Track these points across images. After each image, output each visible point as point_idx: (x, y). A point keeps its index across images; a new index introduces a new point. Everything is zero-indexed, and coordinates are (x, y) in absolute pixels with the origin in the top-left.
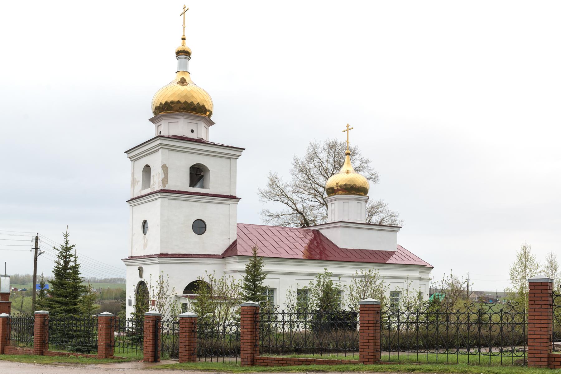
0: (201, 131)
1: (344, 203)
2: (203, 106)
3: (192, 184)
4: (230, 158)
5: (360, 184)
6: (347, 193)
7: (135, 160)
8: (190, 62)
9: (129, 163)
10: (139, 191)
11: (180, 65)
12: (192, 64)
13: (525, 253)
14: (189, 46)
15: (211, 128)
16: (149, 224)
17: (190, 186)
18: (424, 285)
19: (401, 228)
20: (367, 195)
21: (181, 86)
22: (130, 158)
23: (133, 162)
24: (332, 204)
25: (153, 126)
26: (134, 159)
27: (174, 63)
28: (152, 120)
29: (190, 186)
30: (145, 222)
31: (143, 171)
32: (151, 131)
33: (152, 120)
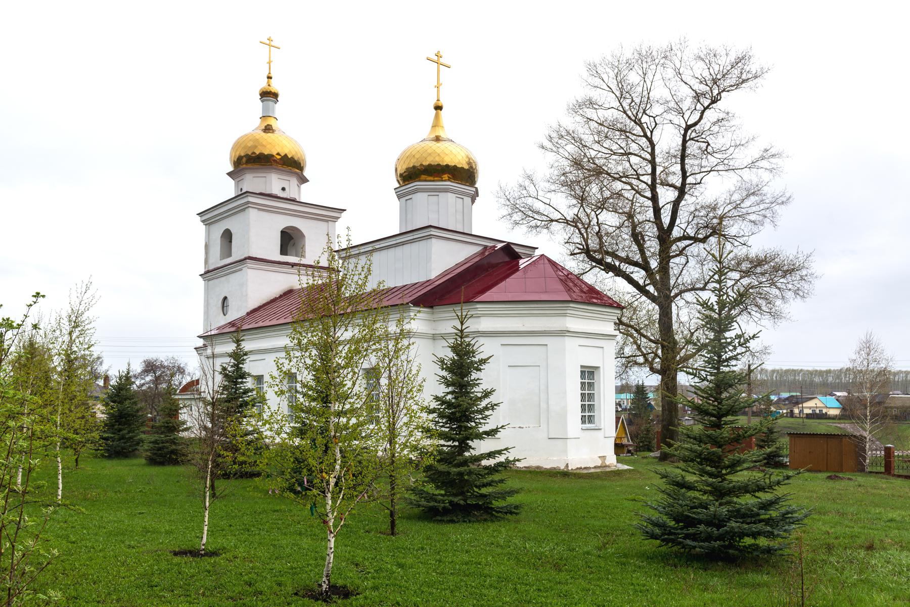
0: (293, 190)
1: (430, 197)
2: (300, 164)
3: (284, 251)
4: (327, 221)
5: (461, 161)
6: (436, 179)
7: (209, 224)
8: (277, 106)
9: (202, 227)
10: (216, 261)
11: (265, 109)
12: (279, 108)
13: (490, 393)
14: (275, 87)
15: (304, 186)
16: (231, 302)
17: (282, 253)
18: (601, 349)
19: (536, 250)
20: (476, 186)
21: (264, 134)
22: (203, 221)
23: (207, 226)
24: (408, 201)
25: (231, 182)
26: (208, 223)
27: (257, 106)
28: (230, 174)
29: (282, 253)
30: (225, 298)
31: (221, 237)
32: (228, 189)
33: (230, 174)
